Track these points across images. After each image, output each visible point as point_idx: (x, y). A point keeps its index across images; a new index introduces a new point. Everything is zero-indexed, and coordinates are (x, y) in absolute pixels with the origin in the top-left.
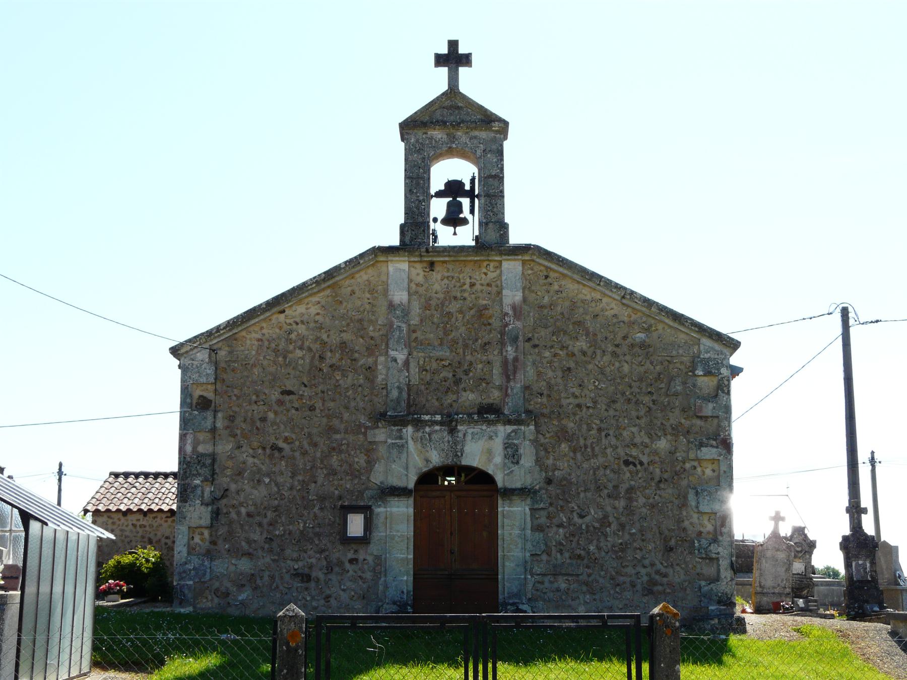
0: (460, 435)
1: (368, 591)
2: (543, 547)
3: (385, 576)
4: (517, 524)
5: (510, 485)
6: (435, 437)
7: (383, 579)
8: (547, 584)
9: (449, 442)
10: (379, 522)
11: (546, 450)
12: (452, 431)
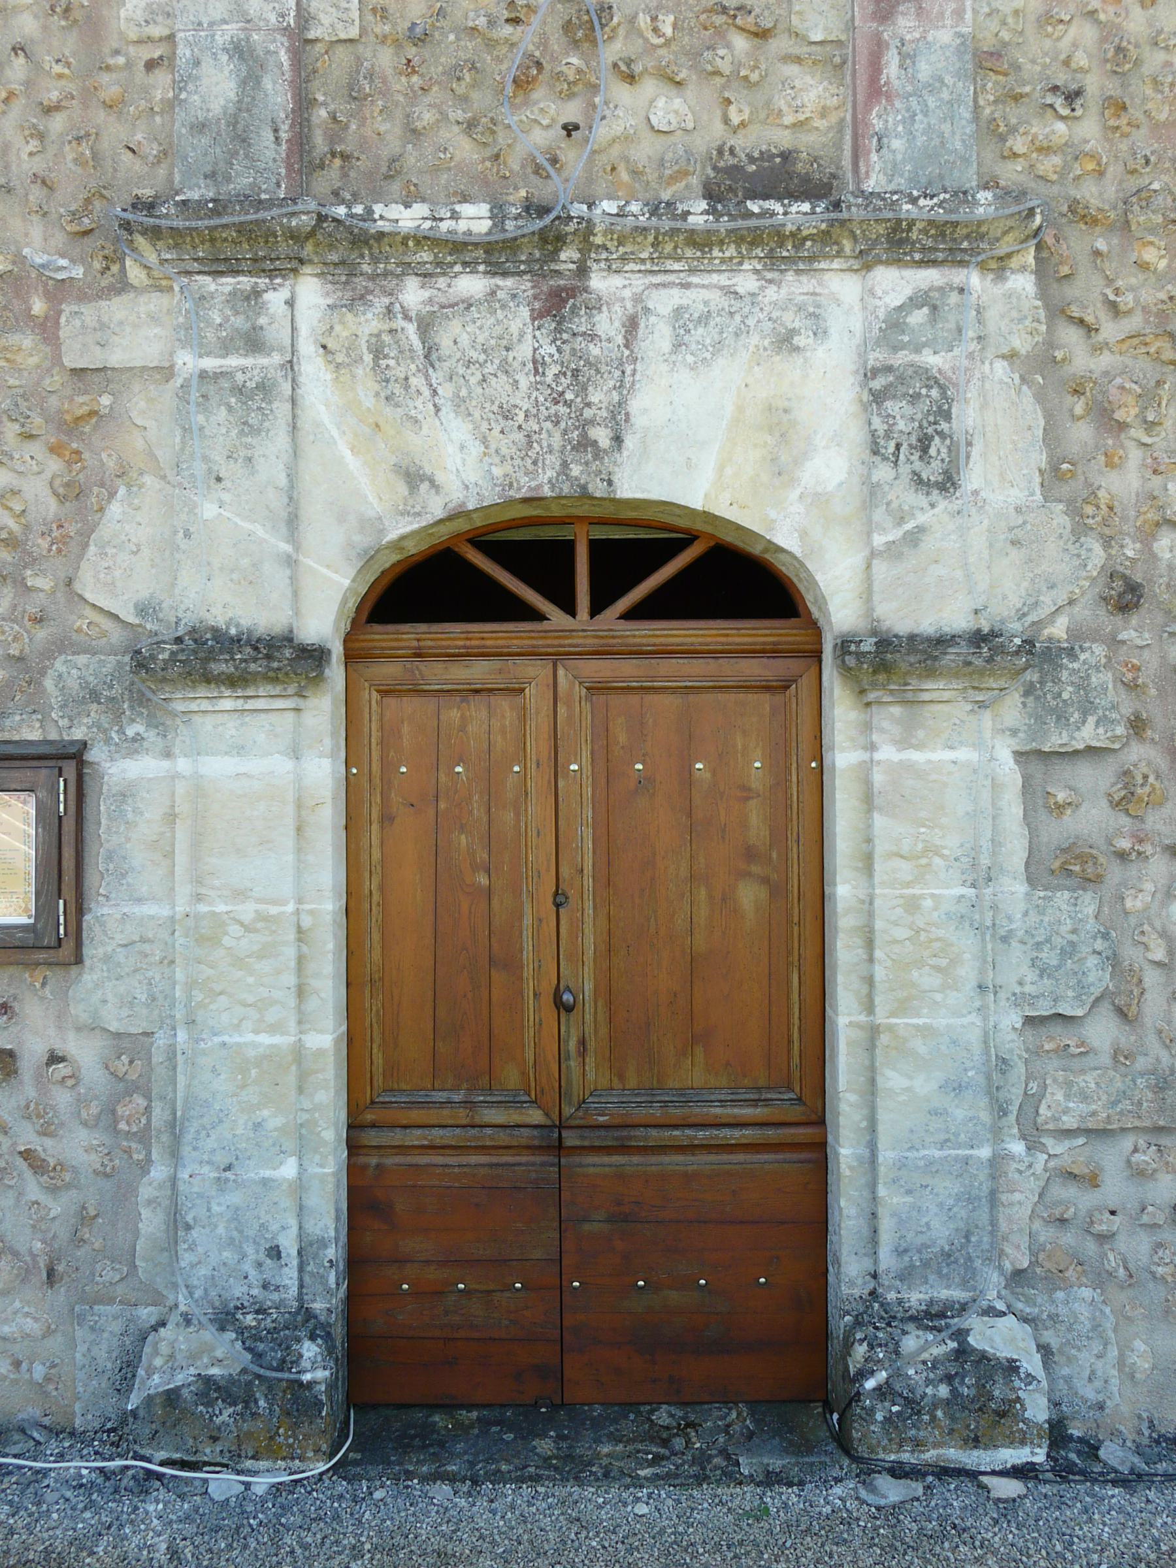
0: (608, 324)
1: (77, 1240)
2: (1098, 977)
3: (175, 1154)
4: (952, 843)
5: (905, 616)
6: (454, 335)
7: (159, 1172)
8: (1115, 1187)
9: (538, 365)
10: (126, 838)
11: (1108, 420)
12: (559, 304)
